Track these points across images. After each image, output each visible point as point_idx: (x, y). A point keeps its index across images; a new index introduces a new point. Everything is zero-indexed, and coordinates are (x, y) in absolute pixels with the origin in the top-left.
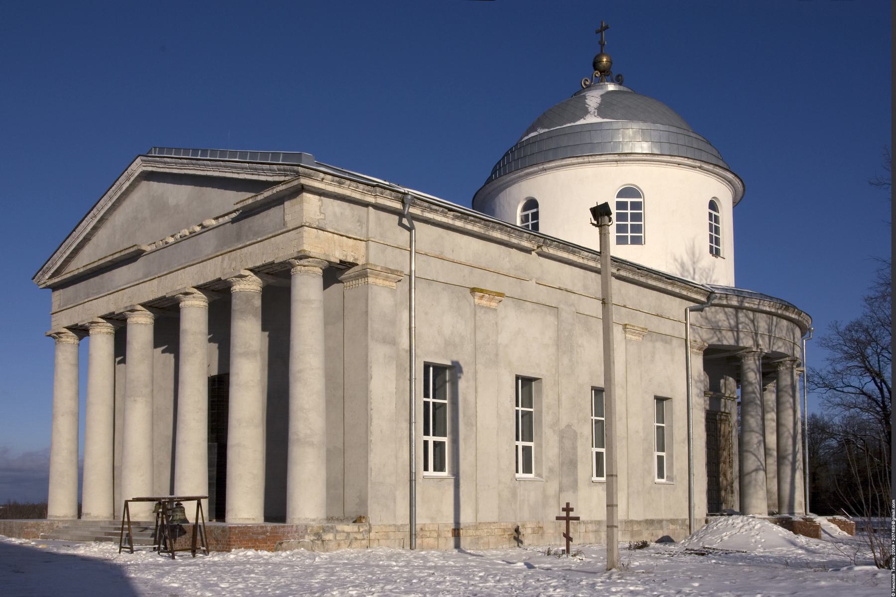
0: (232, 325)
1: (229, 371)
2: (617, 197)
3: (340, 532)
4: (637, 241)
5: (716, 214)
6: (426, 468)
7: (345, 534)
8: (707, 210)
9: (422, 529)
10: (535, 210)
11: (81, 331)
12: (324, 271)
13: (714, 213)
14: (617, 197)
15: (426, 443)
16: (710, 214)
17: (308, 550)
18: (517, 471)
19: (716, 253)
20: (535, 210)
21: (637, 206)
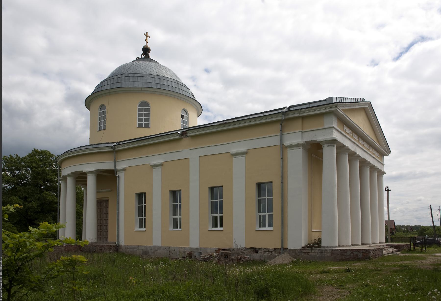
21: (148, 110)
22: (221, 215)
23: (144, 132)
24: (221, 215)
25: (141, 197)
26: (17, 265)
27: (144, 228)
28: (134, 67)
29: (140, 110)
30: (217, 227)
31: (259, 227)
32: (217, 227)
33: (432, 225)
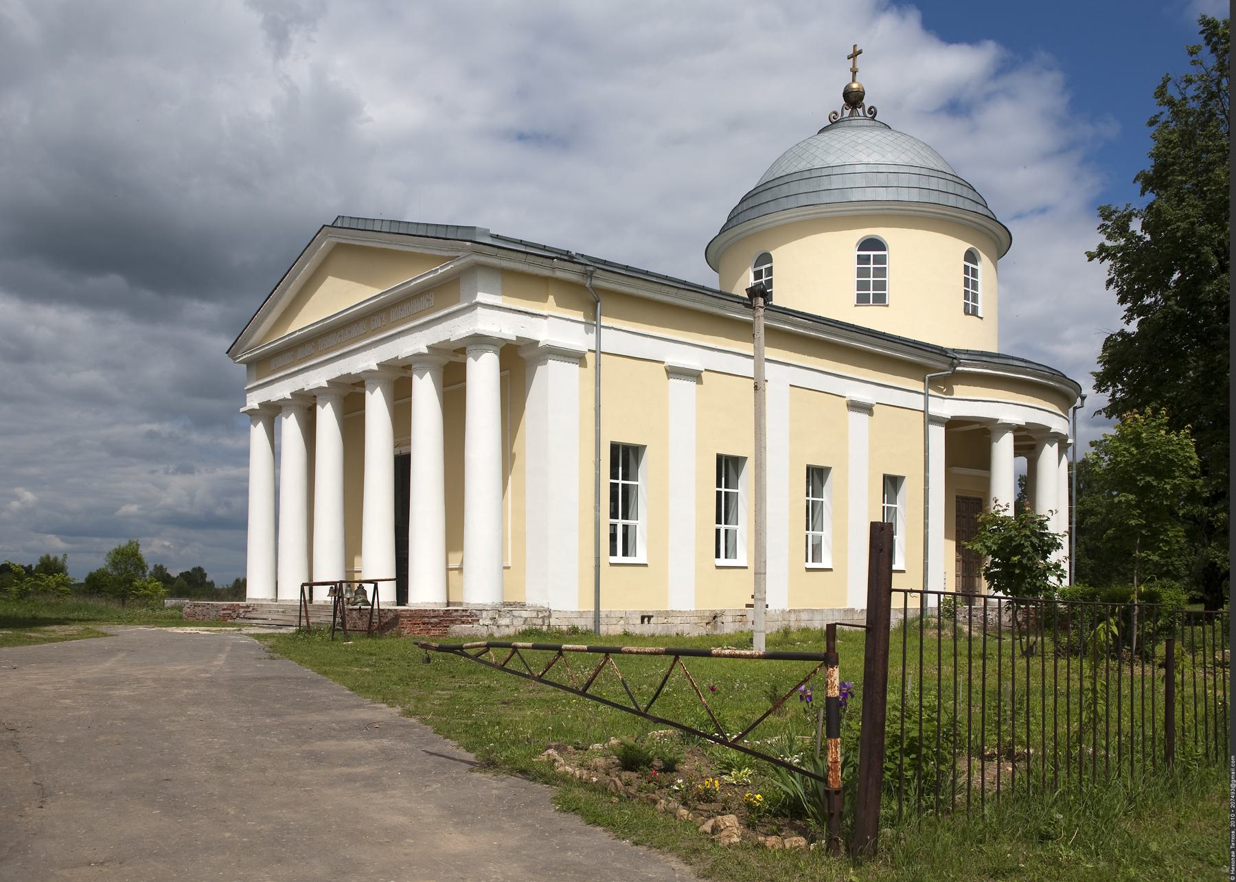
0: (265, 429)
1: (410, 450)
2: (858, 250)
3: (517, 617)
4: (880, 300)
5: (974, 266)
6: (613, 552)
7: (523, 620)
8: (962, 263)
9: (607, 616)
10: (769, 265)
11: (306, 406)
12: (501, 350)
13: (971, 265)
14: (858, 250)
15: (614, 526)
16: (966, 268)
17: (841, 691)
18: (807, 561)
19: (970, 311)
20: (769, 265)
21: (881, 260)
22: (719, 489)
23: (869, 318)
24: (719, 489)
25: (816, 476)
26: (434, 644)
27: (716, 558)
28: (827, 142)
29: (862, 260)
30: (616, 555)
31: (716, 558)
32: (616, 555)
33: (395, 581)
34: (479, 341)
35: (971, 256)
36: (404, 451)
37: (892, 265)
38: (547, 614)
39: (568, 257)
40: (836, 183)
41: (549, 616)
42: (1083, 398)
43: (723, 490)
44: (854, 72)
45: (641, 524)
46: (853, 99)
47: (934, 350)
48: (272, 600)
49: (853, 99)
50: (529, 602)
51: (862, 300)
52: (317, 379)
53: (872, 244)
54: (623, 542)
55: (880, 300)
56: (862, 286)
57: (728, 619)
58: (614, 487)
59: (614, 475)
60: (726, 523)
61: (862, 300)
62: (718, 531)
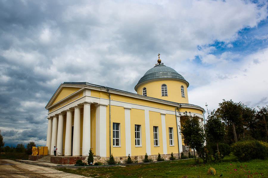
4: (166, 95)
6: (114, 145)
16: (181, 89)
23: (164, 98)
34: (86, 103)
35: (182, 87)
36: (73, 126)
37: (168, 89)
38: (100, 158)
39: (104, 87)
40: (157, 75)
41: (100, 158)
42: (205, 111)
43: (137, 131)
44: (159, 57)
45: (121, 138)
46: (159, 62)
47: (96, 86)
48: (70, 156)
49: (159, 62)
50: (96, 155)
51: (163, 95)
52: (59, 112)
53: (164, 85)
54: (138, 143)
55: (166, 95)
56: (163, 93)
57: (138, 158)
58: (114, 132)
59: (114, 129)
60: (138, 138)
61: (163, 95)
62: (136, 140)
